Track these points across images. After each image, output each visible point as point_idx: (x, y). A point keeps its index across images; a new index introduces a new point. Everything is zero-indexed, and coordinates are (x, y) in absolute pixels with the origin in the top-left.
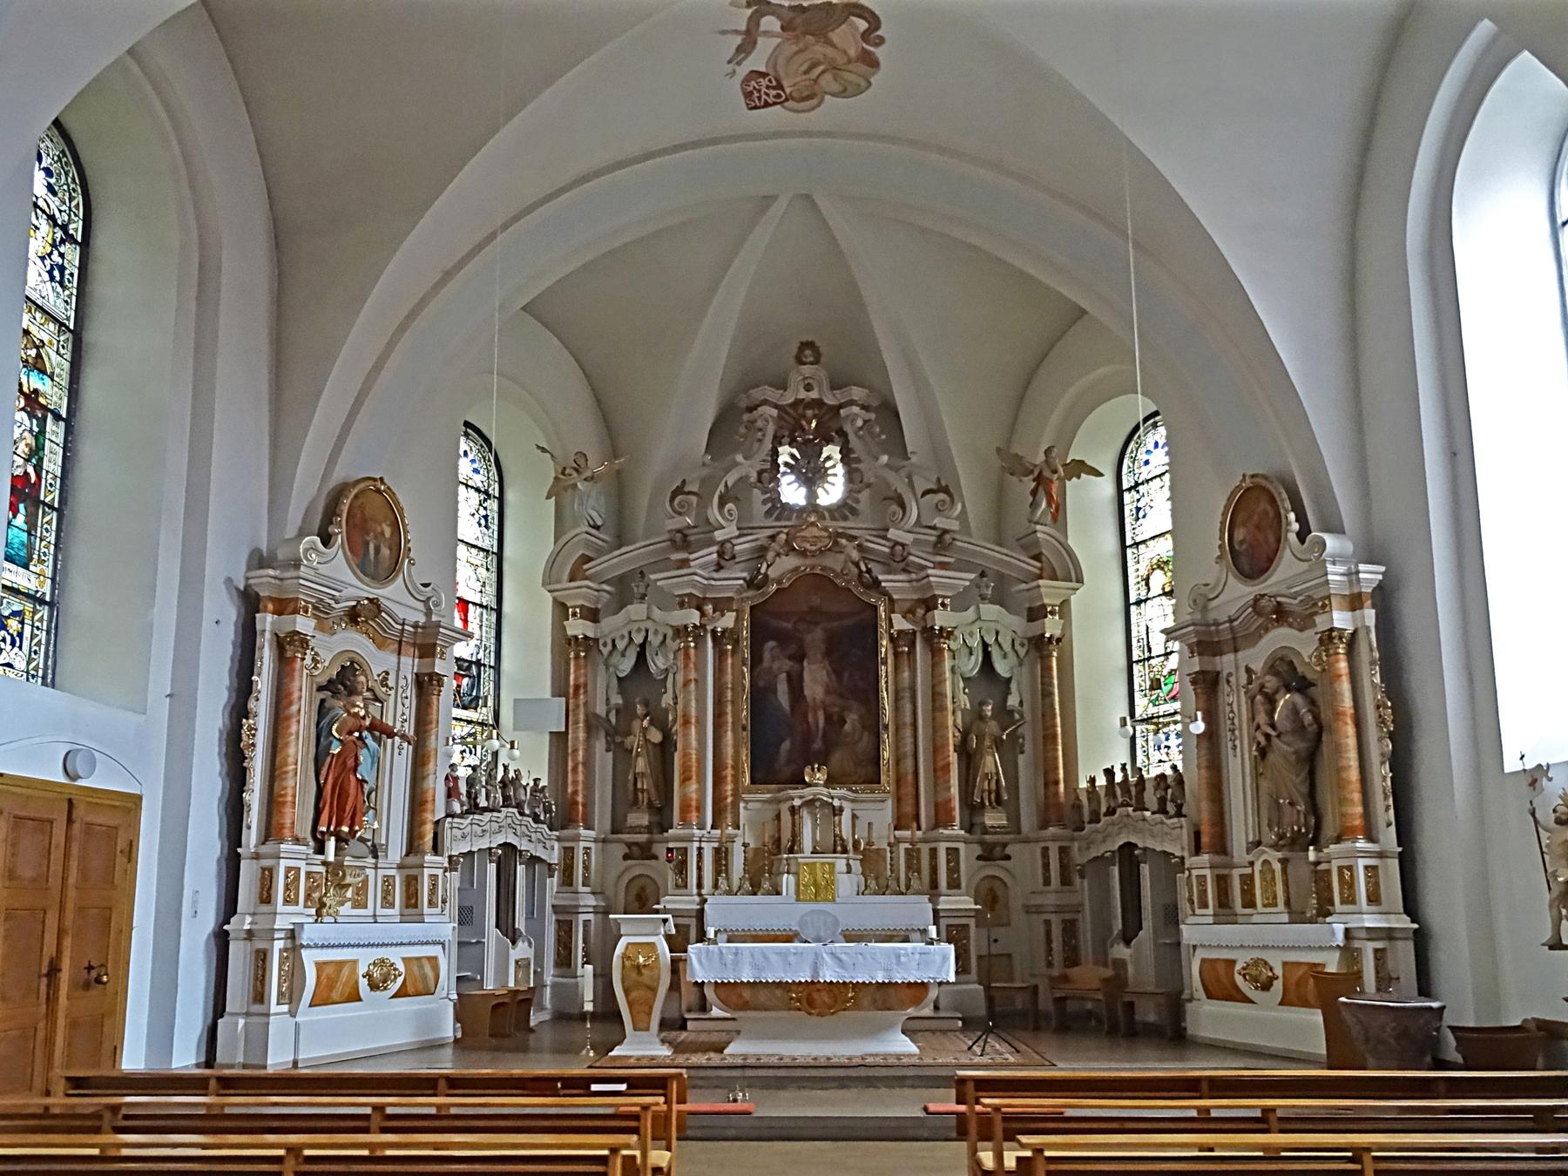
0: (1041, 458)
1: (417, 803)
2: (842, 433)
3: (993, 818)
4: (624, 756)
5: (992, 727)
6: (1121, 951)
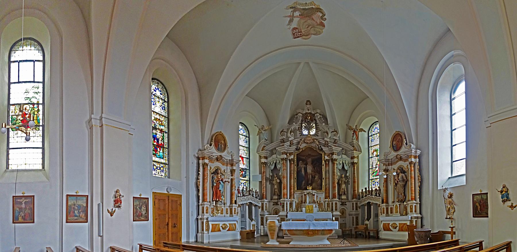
0: (355, 127)
1: (232, 195)
2: (315, 120)
3: (344, 197)
4: (272, 185)
5: (344, 179)
6: (367, 222)
